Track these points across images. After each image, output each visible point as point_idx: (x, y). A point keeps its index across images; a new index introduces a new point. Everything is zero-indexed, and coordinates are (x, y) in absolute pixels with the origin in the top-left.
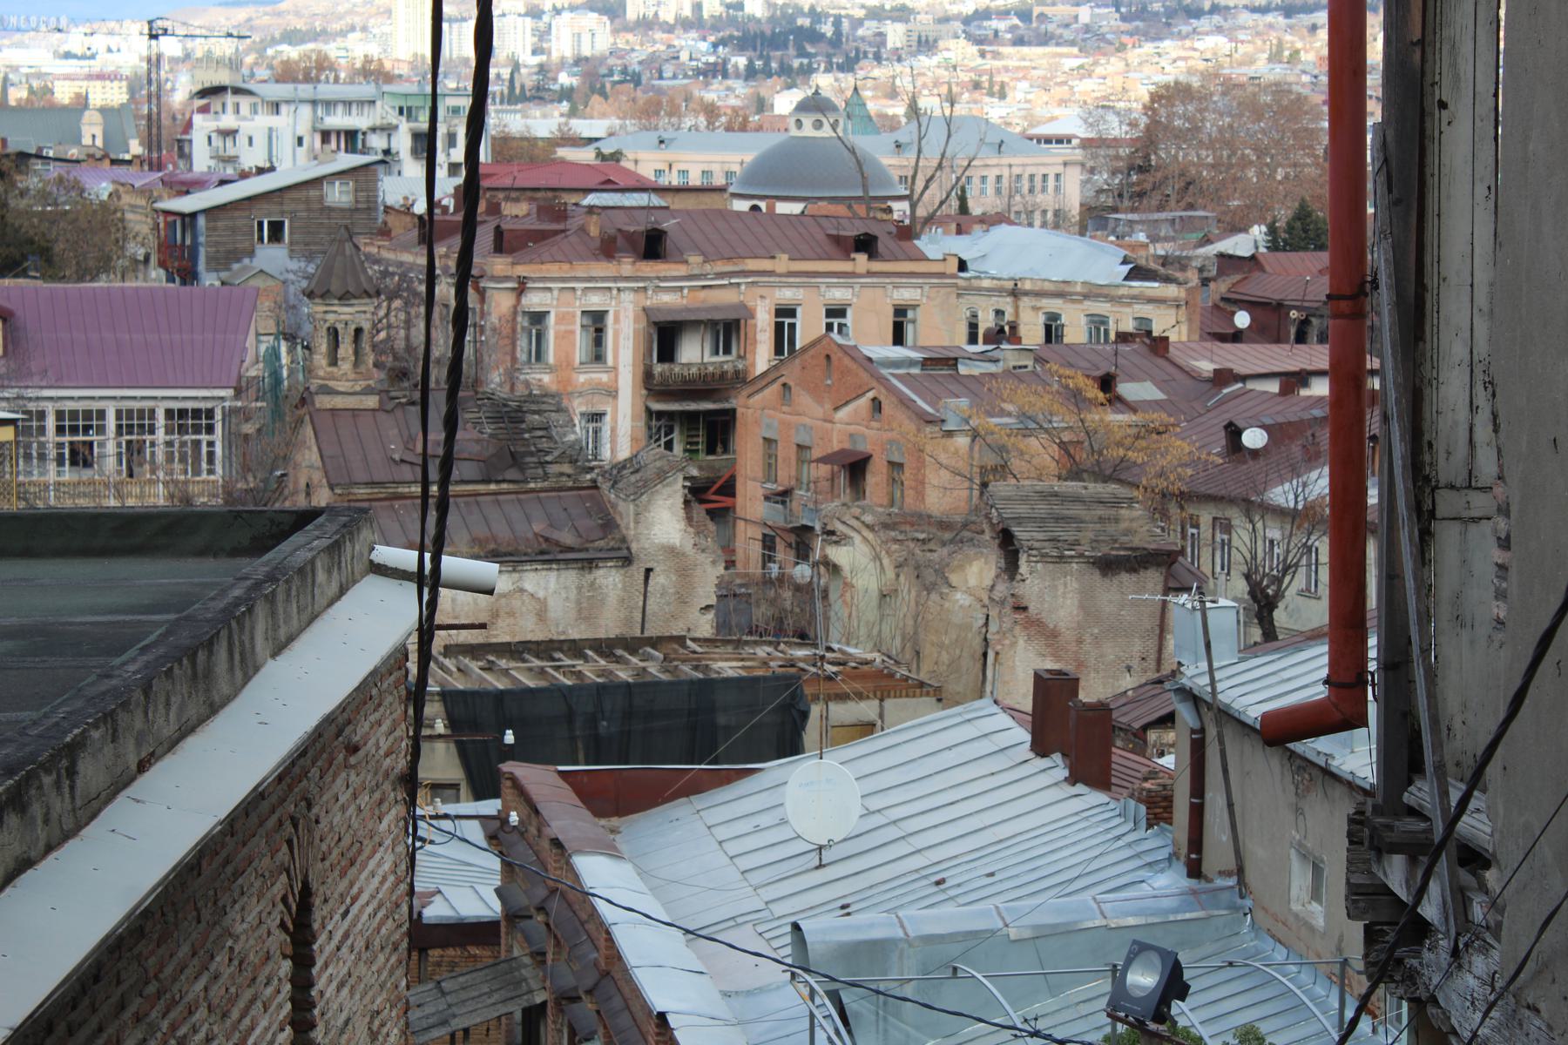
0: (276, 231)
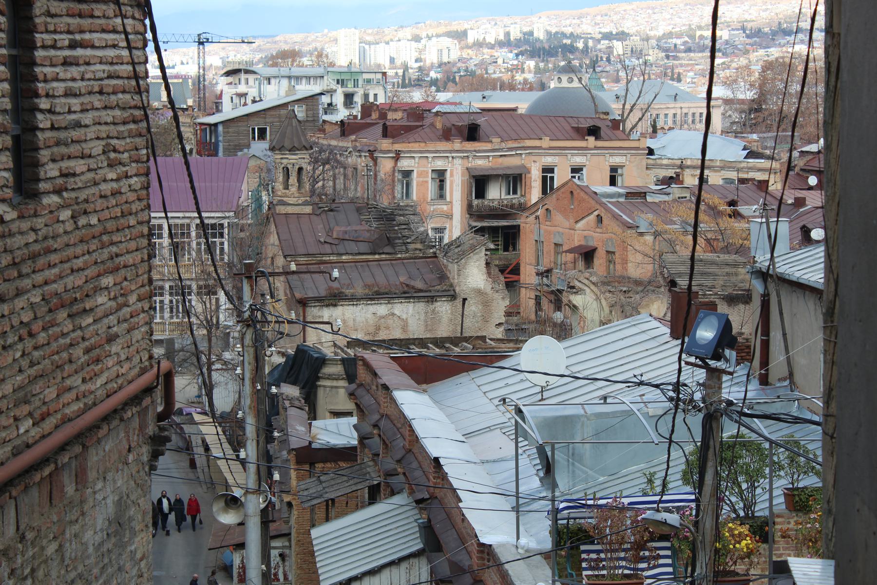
0: (262, 133)
